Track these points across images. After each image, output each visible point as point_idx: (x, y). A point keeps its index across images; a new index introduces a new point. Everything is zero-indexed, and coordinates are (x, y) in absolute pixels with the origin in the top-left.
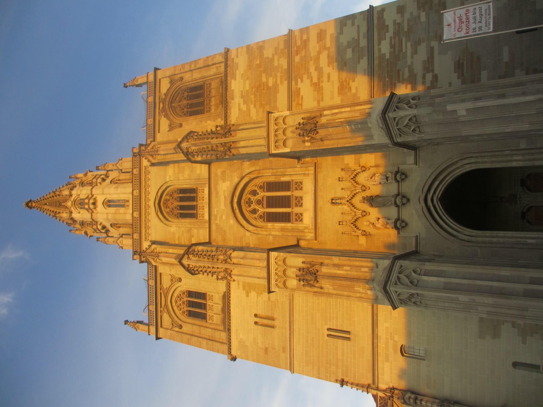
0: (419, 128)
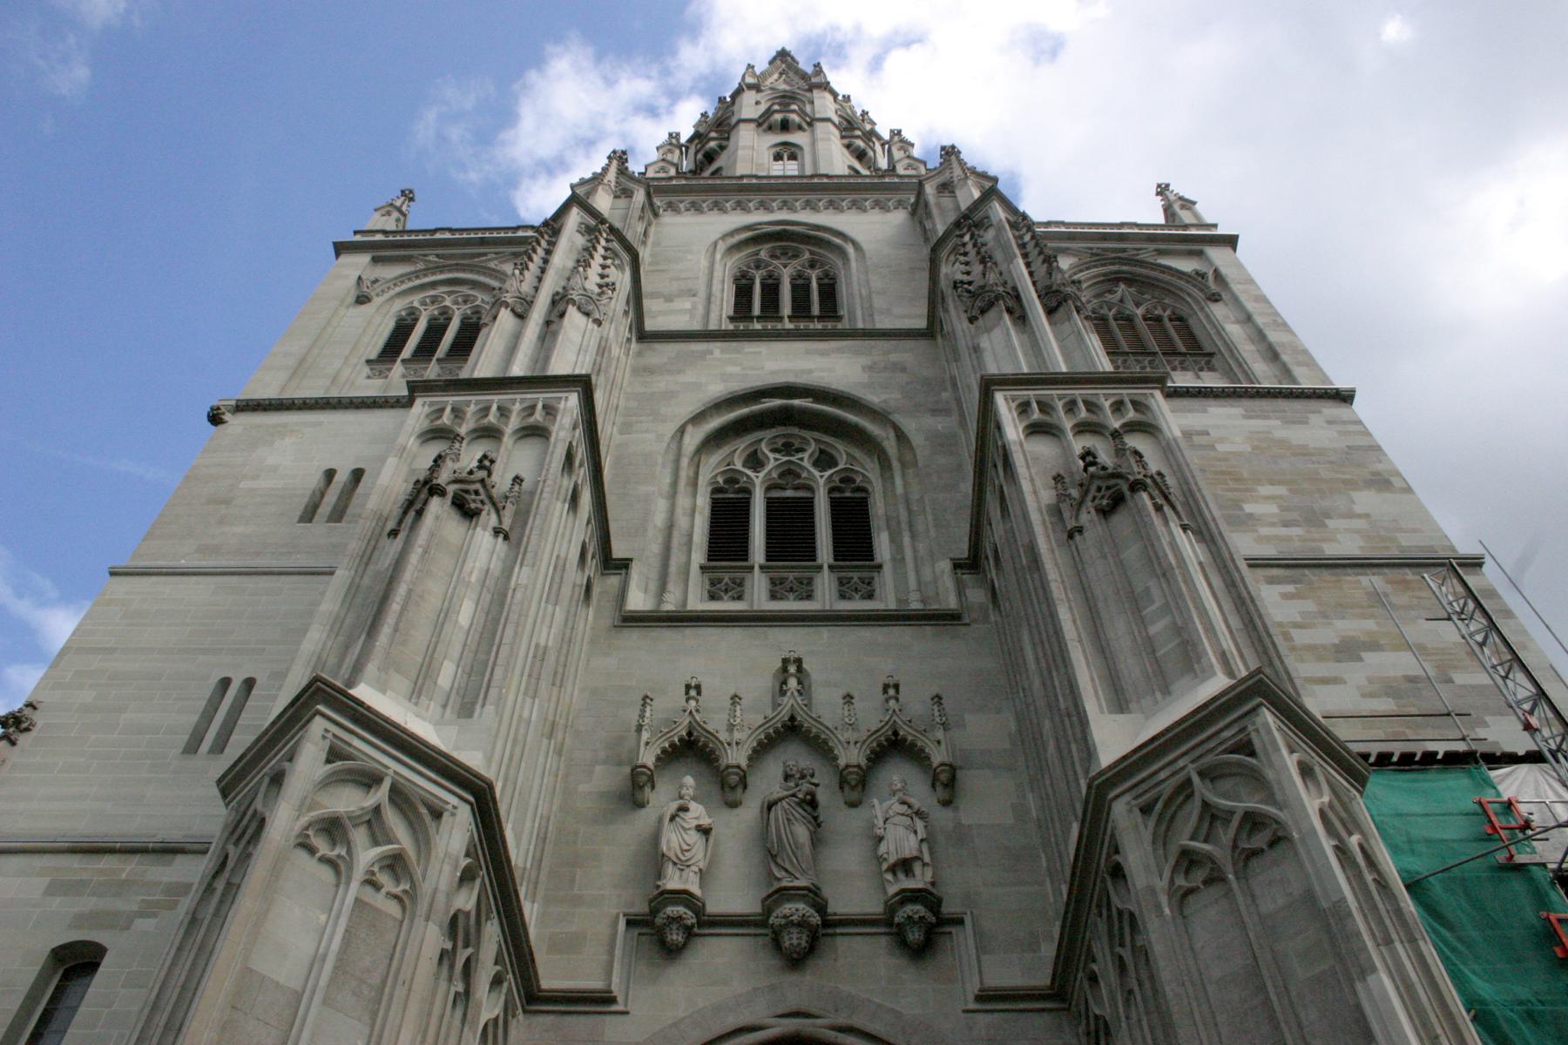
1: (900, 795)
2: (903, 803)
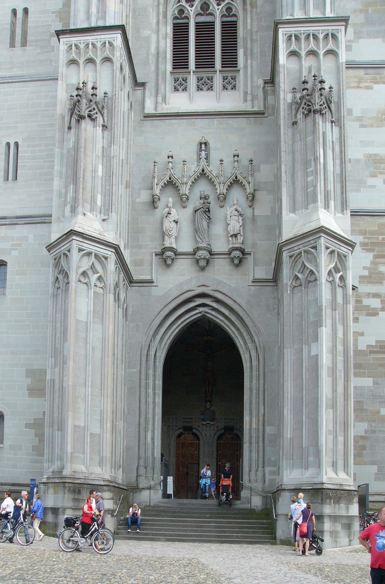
0: (300, 286)
1: (235, 207)
2: (236, 210)
